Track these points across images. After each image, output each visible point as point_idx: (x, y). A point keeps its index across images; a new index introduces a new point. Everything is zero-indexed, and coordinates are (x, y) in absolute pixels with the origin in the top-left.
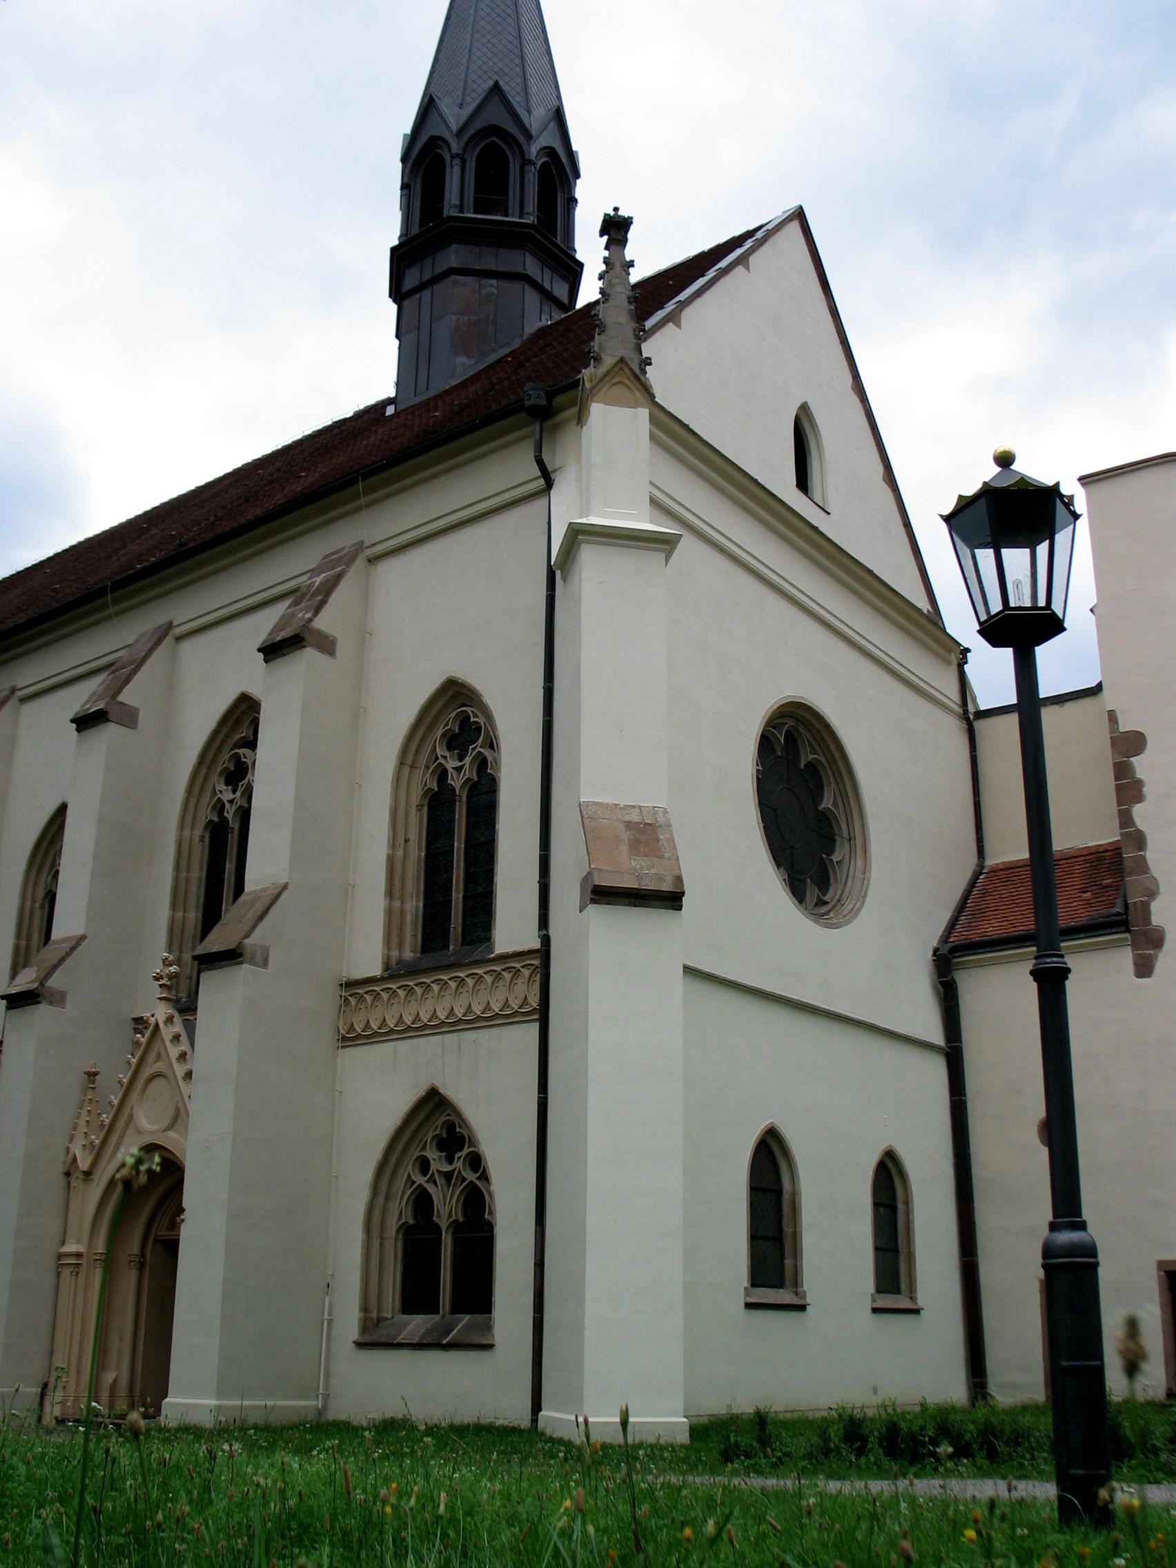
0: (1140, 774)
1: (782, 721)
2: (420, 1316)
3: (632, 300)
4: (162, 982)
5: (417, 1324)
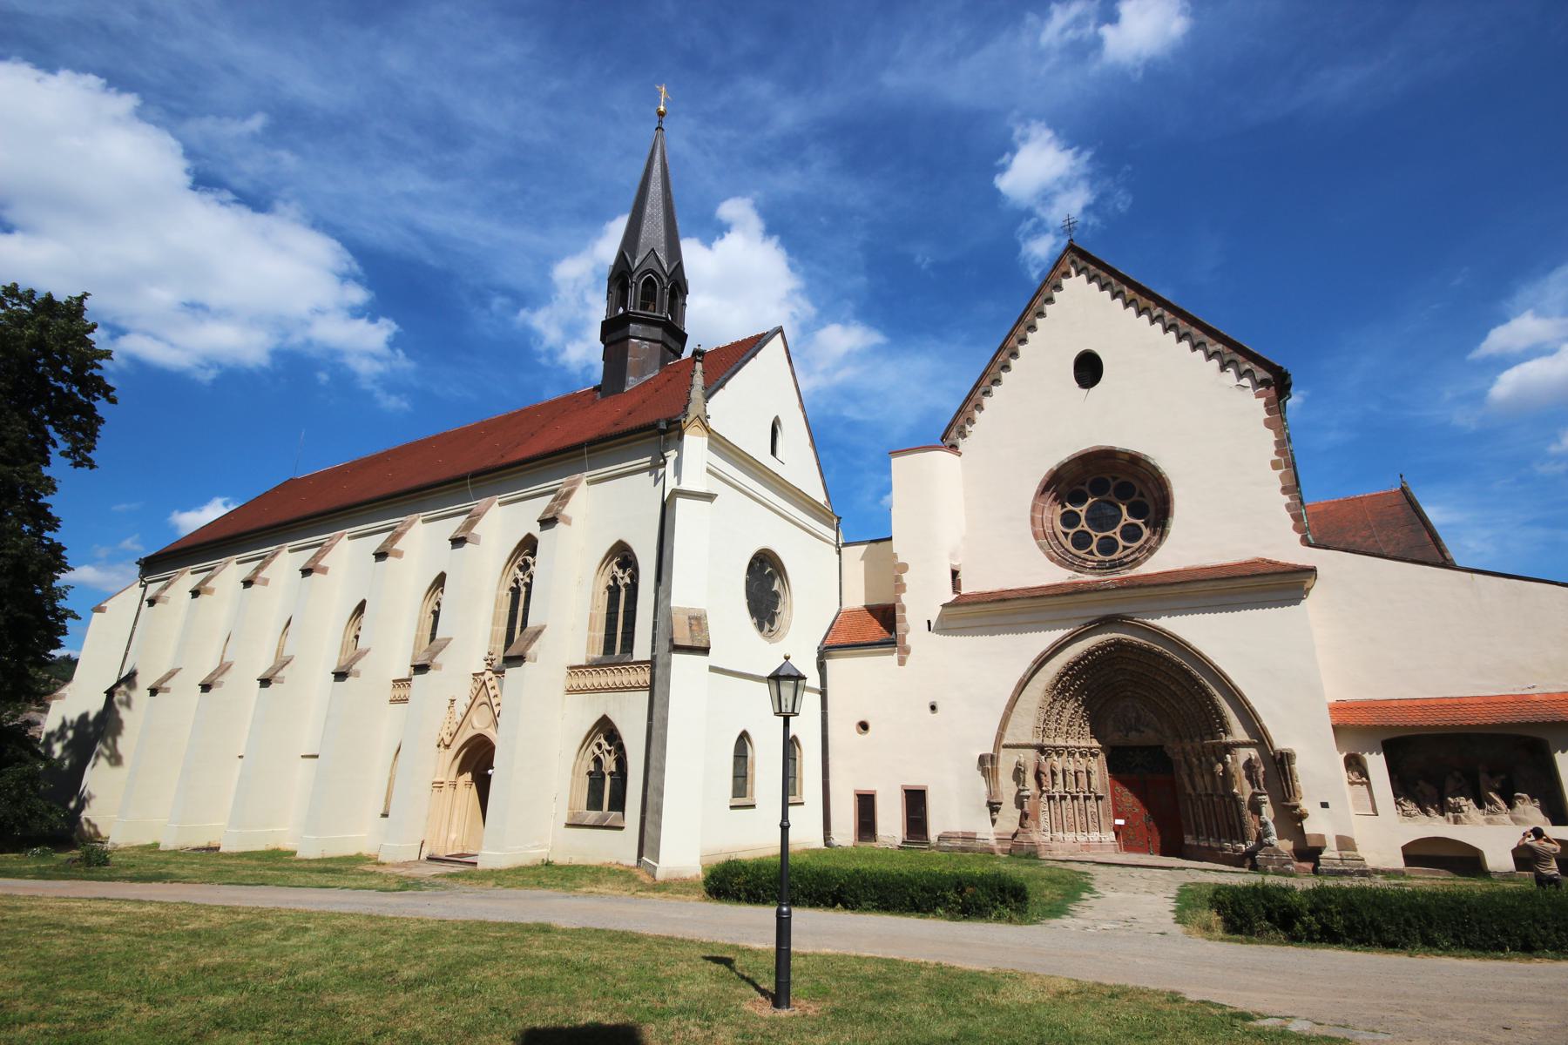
0: (905, 581)
5: (593, 816)
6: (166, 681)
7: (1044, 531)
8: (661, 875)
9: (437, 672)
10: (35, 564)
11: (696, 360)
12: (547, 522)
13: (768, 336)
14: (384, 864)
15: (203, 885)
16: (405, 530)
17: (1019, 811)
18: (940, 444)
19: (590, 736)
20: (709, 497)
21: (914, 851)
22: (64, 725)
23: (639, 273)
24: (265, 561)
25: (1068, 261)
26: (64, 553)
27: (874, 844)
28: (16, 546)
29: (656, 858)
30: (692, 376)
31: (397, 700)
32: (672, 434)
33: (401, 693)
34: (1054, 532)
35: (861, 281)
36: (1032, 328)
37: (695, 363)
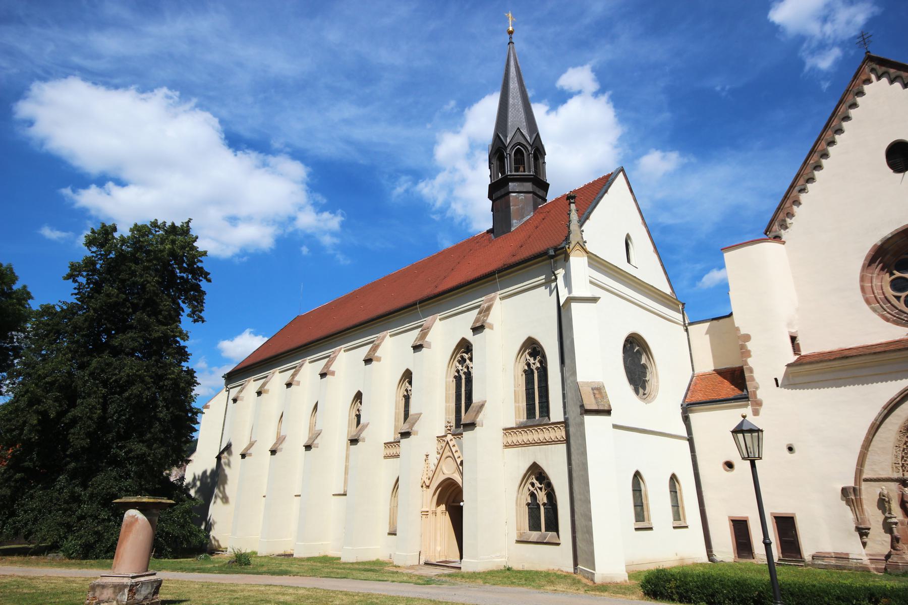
0: (749, 348)
4: (448, 428)
5: (534, 536)
6: (249, 449)
7: (875, 297)
8: (598, 579)
9: (416, 436)
10: (183, 383)
11: (570, 203)
12: (478, 329)
13: (614, 175)
14: (399, 567)
15: (311, 578)
16: (381, 343)
17: (889, 536)
18: (765, 237)
19: (525, 477)
20: (594, 300)
21: (791, 567)
22: (194, 479)
23: (510, 147)
24: (297, 369)
25: (867, 69)
26: (195, 375)
27: (752, 560)
28: (173, 372)
29: (592, 565)
30: (569, 214)
31: (388, 456)
32: (558, 257)
33: (392, 451)
34: (886, 297)
35: (666, 116)
36: (840, 131)
37: (569, 204)
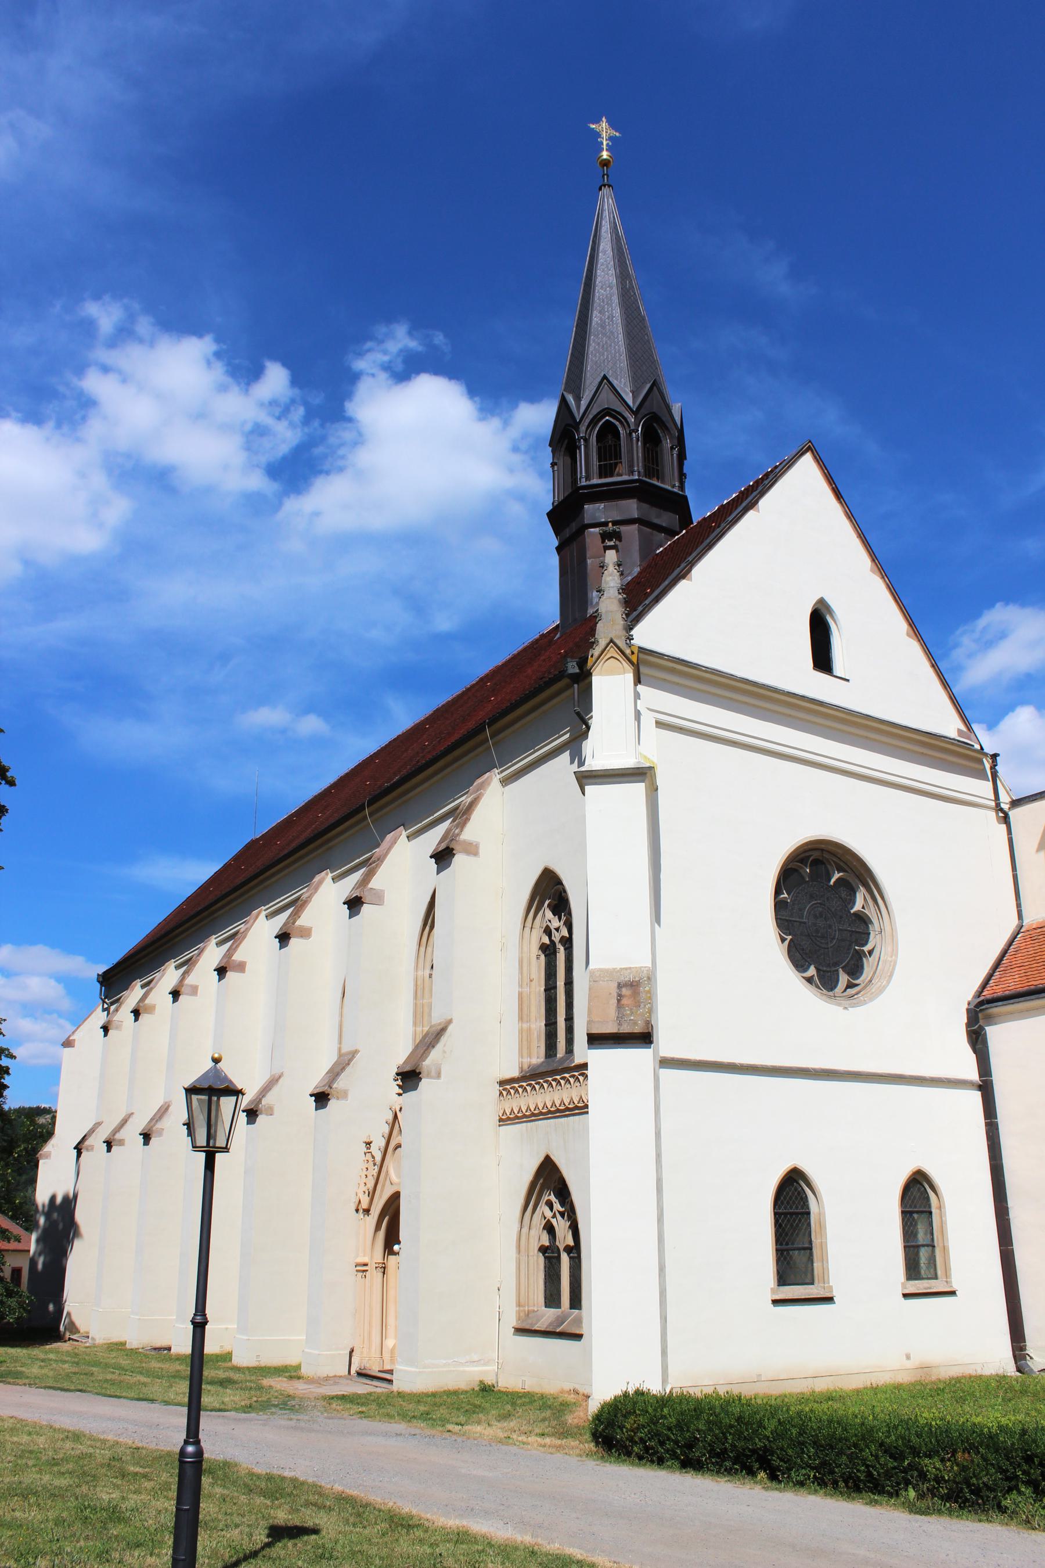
1: (807, 854)
2: (552, 1310)
3: (621, 591)
9: (341, 1102)
